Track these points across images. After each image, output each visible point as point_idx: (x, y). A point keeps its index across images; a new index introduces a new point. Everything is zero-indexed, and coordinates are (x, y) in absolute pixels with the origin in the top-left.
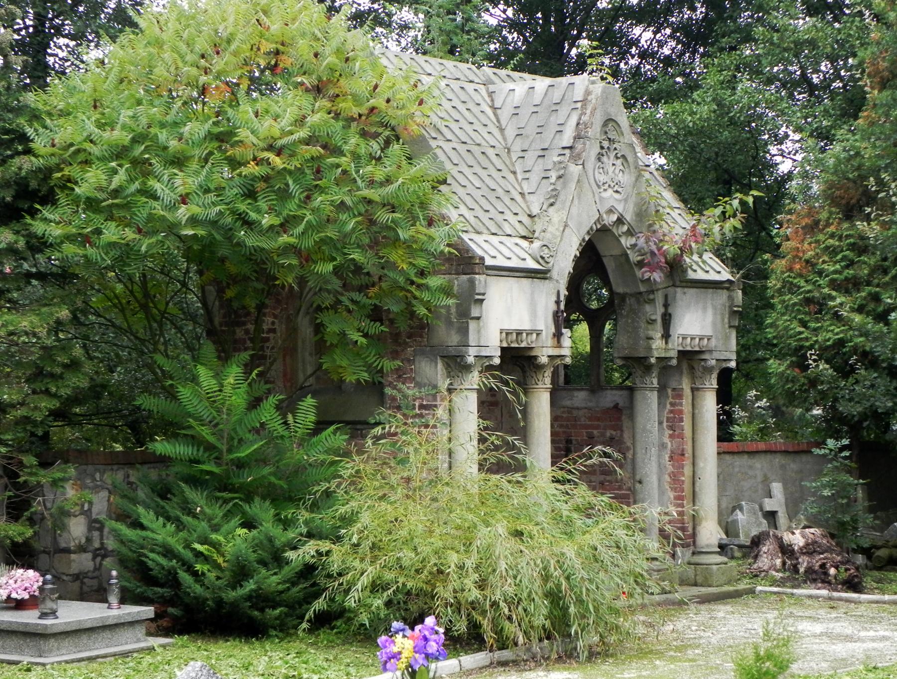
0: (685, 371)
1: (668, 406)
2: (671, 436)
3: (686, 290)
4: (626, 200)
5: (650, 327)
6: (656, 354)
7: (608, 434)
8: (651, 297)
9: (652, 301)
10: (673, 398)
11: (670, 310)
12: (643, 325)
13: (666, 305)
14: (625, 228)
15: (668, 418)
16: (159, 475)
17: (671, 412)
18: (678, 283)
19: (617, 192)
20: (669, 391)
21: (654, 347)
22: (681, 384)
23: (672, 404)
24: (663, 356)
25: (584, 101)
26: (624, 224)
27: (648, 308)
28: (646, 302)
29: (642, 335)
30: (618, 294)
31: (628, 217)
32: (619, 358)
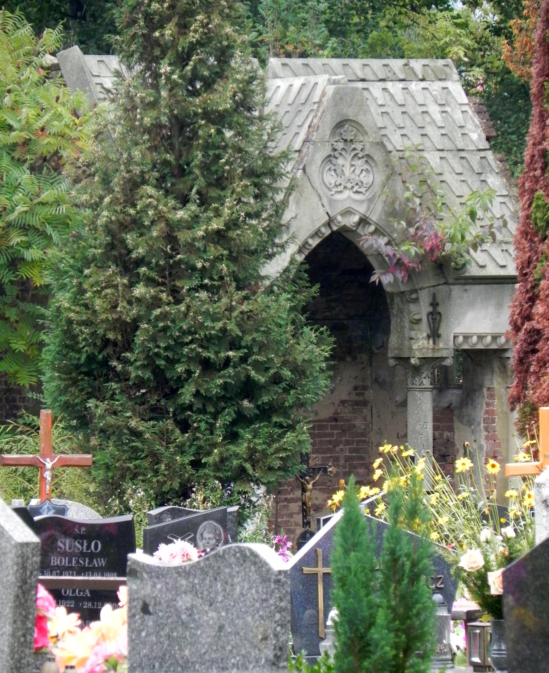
0: (496, 369)
1: (485, 406)
2: (487, 438)
3: (467, 287)
4: (371, 201)
5: (415, 327)
6: (418, 355)
7: (445, 436)
8: (414, 296)
9: (416, 300)
10: (487, 398)
11: (440, 309)
12: (407, 325)
13: (434, 304)
14: (372, 228)
15: (484, 420)
16: (333, 500)
17: (487, 412)
18: (451, 281)
19: (357, 192)
20: (485, 390)
21: (415, 347)
22: (492, 384)
23: (488, 405)
24: (430, 355)
25: (320, 102)
26: (370, 224)
27: (412, 307)
28: (409, 302)
29: (407, 335)
30: (388, 293)
31: (374, 217)
32: (392, 358)
